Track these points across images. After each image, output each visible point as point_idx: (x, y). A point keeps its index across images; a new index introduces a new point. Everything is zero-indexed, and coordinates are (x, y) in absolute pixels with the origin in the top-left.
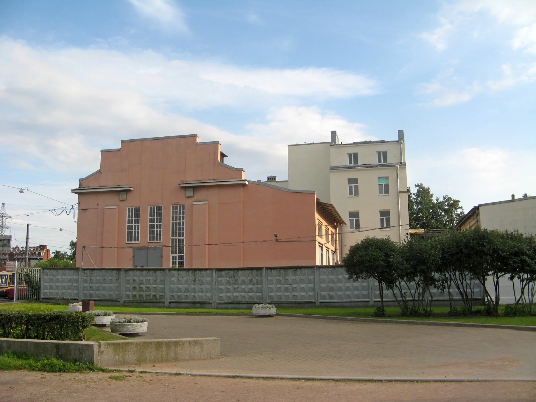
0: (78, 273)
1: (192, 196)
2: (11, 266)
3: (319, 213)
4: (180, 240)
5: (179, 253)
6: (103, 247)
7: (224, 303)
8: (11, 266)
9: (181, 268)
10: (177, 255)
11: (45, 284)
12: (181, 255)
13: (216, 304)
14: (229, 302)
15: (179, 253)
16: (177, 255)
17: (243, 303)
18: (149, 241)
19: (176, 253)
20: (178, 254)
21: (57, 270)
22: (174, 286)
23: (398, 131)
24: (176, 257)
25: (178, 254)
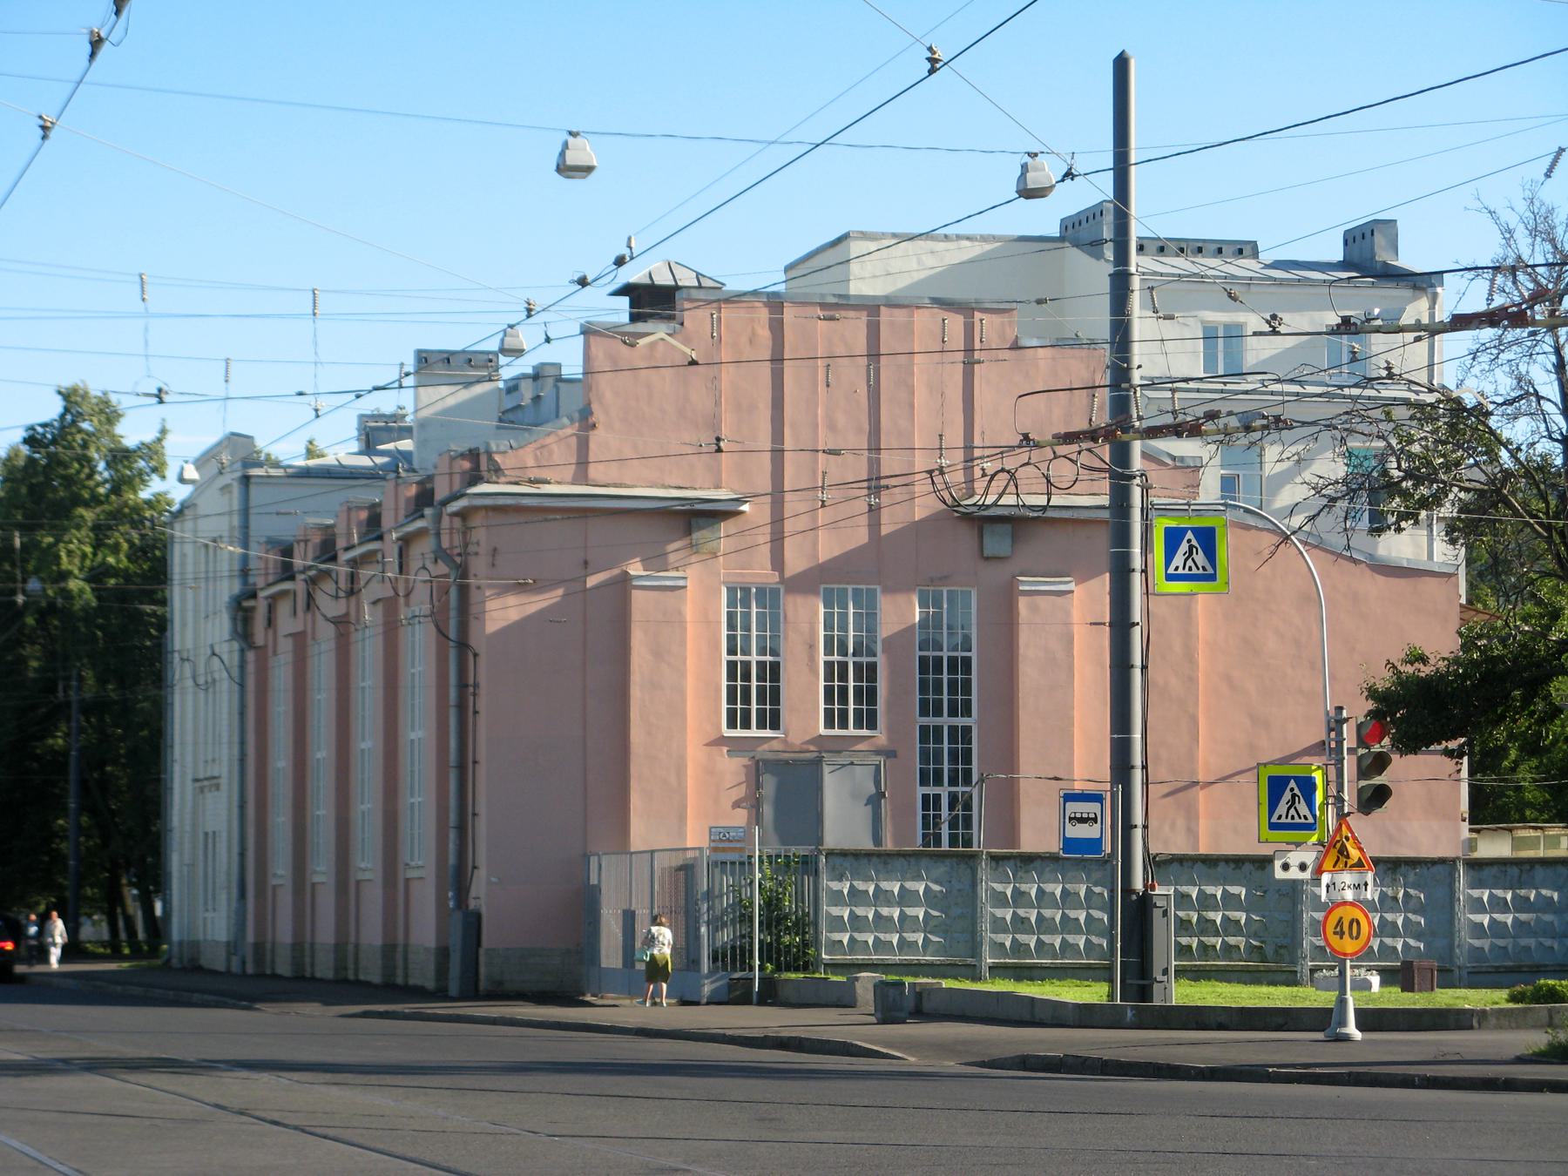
0: (969, 870)
1: (1008, 554)
2: (732, 845)
3: (328, 470)
4: (953, 729)
5: (953, 781)
6: (1061, 779)
7: (1490, 970)
8: (732, 845)
9: (961, 849)
10: (944, 792)
11: (835, 911)
12: (960, 789)
13: (1464, 973)
14: (1505, 967)
15: (953, 781)
16: (944, 792)
17: (1548, 969)
18: (822, 730)
19: (938, 781)
20: (949, 785)
21: (908, 858)
22: (1485, 919)
23: (1395, 221)
24: (937, 797)
25: (949, 785)
